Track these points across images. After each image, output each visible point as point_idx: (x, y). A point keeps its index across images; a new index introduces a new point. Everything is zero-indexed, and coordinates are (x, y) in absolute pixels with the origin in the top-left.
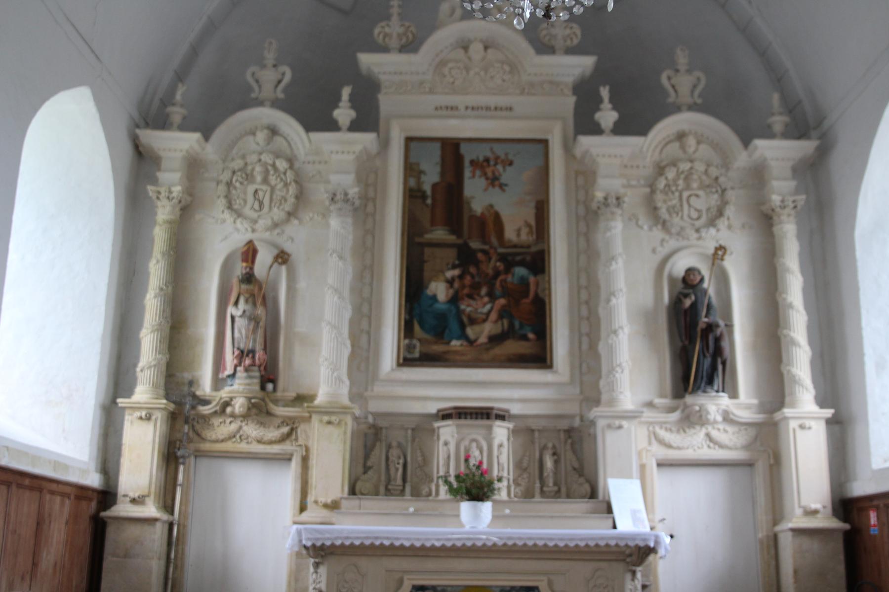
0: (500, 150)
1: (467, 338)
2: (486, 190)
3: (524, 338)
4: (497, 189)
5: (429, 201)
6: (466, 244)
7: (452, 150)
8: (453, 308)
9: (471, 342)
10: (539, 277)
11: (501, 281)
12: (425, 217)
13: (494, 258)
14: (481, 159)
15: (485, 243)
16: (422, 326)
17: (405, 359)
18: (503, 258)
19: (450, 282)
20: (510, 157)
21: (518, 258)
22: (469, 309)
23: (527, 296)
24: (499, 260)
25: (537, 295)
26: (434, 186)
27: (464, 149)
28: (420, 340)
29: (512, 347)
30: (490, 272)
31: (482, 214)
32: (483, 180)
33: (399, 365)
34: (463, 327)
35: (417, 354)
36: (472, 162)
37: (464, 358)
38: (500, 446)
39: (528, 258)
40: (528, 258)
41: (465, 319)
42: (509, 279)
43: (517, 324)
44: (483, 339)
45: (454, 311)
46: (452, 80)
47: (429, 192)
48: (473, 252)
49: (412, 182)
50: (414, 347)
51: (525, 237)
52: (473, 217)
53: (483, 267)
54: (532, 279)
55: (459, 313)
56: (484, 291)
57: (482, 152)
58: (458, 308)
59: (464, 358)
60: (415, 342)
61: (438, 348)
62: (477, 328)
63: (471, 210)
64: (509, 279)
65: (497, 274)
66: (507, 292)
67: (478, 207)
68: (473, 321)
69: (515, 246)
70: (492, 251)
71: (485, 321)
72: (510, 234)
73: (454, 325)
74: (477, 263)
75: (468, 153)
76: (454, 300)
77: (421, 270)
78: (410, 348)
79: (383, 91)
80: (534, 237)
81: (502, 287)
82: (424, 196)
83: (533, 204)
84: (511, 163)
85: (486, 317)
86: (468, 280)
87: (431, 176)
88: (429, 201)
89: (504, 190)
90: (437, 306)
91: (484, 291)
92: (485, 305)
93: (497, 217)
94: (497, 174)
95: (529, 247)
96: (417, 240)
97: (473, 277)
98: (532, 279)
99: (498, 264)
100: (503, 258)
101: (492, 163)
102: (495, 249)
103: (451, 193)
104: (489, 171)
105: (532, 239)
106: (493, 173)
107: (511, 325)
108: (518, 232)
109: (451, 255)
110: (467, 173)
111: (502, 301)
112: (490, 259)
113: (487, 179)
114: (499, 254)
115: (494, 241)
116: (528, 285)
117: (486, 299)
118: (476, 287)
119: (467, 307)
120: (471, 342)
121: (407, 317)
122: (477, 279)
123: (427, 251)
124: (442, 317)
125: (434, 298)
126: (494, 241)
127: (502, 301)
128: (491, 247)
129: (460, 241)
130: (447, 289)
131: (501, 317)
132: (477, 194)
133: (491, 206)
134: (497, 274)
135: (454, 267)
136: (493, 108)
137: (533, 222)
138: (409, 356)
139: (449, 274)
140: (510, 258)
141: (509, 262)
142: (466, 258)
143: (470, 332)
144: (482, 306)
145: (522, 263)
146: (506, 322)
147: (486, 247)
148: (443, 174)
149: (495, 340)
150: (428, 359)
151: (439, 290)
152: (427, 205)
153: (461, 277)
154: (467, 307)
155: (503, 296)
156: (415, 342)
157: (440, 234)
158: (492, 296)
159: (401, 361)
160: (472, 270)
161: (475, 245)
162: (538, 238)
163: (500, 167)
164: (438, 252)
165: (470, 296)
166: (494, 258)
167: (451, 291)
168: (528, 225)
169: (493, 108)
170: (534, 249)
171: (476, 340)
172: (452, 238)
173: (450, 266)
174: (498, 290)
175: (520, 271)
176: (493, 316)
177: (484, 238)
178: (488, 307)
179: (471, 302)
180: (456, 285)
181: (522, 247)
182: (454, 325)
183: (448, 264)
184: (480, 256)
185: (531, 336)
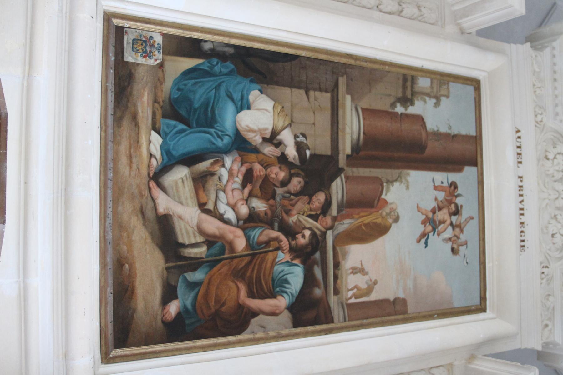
0: (470, 232)
1: (165, 169)
2: (419, 209)
3: (170, 293)
4: (421, 229)
5: (399, 109)
6: (339, 171)
7: (462, 154)
8: (226, 140)
9: (156, 178)
10: (286, 317)
11: (277, 239)
12: (378, 99)
13: (317, 225)
14: (459, 201)
15: (340, 208)
16: (189, 73)
17: (120, 31)
18: (317, 242)
19: (272, 139)
20: (462, 249)
21: (318, 272)
22: (224, 173)
23: (251, 295)
24: (313, 235)
25: (254, 314)
26: (419, 119)
27: (470, 171)
28: (161, 66)
29: (149, 267)
30: (292, 219)
31: (386, 202)
32: (433, 204)
33: (108, 17)
34: (190, 160)
35: (129, 57)
36: (454, 185)
37: (124, 160)
38: (216, 140)
39: (318, 292)
40: (318, 292)
41: (204, 166)
42: (282, 256)
43: (198, 276)
44: (164, 204)
45: (220, 143)
46: (551, 156)
47: (412, 110)
48: (325, 186)
49: (423, 83)
50: (146, 55)
51: (352, 282)
52: (379, 183)
53: (301, 204)
54: (283, 302)
55: (216, 154)
56: (260, 205)
57: (466, 201)
58: (227, 151)
59: (124, 160)
60: (158, 56)
61: (144, 104)
62: (187, 190)
63: (390, 182)
64: (282, 256)
65: (290, 232)
66: (257, 251)
67: (394, 194)
68: (200, 181)
69: (337, 265)
70: (328, 220)
71: (202, 206)
72: (356, 254)
73: (193, 141)
74: (307, 192)
75: (465, 177)
76: (241, 144)
77: (292, 84)
78: (144, 45)
79: (533, 53)
80: (353, 301)
81: (267, 243)
82: (406, 101)
83: (401, 295)
84: (454, 251)
85: (206, 210)
86: (278, 173)
87: (438, 117)
88: (399, 109)
89: (419, 241)
90: (230, 108)
91: (260, 205)
92: (233, 207)
93: (380, 230)
94: (441, 227)
95: (337, 292)
96: (342, 81)
97: (284, 183)
98: (283, 302)
99: (307, 233)
100: (317, 242)
101: (454, 219)
102: (331, 228)
103: (401, 148)
104: (442, 215)
105: (349, 296)
106: (442, 222)
107: (195, 264)
108: (359, 270)
109: (320, 144)
110: (442, 177)
111: (241, 244)
112: (315, 218)
113: (434, 212)
114: (324, 234)
115: (345, 225)
116: (273, 295)
117: (244, 210)
118: (266, 189)
119: (229, 168)
120: (156, 178)
121: (207, 47)
122: (279, 191)
123: (325, 98)
124: (207, 119)
125: (244, 105)
126: (345, 225)
127: (241, 244)
128: (335, 219)
129: (342, 161)
130: (260, 131)
131: (211, 241)
132: (411, 192)
133: (397, 220)
134: (290, 232)
135: (300, 147)
136: (523, 219)
137: (374, 297)
138: (127, 39)
139: (287, 137)
140: (317, 255)
141: (309, 254)
142: (317, 171)
143: (180, 175)
144: (231, 199)
145: (309, 280)
146: (201, 251)
147: (334, 211)
148: (437, 135)
149: (164, 230)
150: (121, 82)
151: (259, 115)
152: (393, 105)
153: (283, 159)
154: (229, 168)
155: (249, 245)
156: (158, 56)
157: (352, 126)
158: (251, 221)
159: (117, 22)
160: (296, 183)
161: (338, 188)
162: (351, 306)
163: (449, 233)
164: (323, 119)
165: (248, 178)
166: (317, 225)
167: (257, 140)
168: (369, 291)
169: (523, 219)
170: (333, 300)
171: (160, 186)
172: (346, 147)
173: (301, 139)
174: (262, 234)
175: (296, 278)
176: (212, 226)
177: (352, 204)
178: (230, 215)
179: (239, 179)
180: (269, 150)
181: (336, 277)
182: (193, 141)
183: (304, 135)
184: (320, 197)
185: (173, 308)
